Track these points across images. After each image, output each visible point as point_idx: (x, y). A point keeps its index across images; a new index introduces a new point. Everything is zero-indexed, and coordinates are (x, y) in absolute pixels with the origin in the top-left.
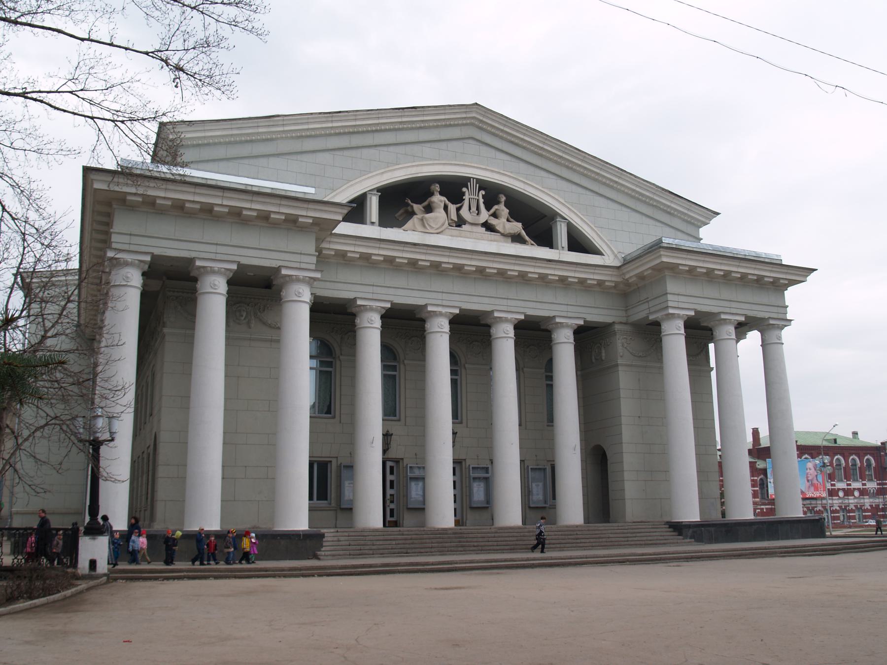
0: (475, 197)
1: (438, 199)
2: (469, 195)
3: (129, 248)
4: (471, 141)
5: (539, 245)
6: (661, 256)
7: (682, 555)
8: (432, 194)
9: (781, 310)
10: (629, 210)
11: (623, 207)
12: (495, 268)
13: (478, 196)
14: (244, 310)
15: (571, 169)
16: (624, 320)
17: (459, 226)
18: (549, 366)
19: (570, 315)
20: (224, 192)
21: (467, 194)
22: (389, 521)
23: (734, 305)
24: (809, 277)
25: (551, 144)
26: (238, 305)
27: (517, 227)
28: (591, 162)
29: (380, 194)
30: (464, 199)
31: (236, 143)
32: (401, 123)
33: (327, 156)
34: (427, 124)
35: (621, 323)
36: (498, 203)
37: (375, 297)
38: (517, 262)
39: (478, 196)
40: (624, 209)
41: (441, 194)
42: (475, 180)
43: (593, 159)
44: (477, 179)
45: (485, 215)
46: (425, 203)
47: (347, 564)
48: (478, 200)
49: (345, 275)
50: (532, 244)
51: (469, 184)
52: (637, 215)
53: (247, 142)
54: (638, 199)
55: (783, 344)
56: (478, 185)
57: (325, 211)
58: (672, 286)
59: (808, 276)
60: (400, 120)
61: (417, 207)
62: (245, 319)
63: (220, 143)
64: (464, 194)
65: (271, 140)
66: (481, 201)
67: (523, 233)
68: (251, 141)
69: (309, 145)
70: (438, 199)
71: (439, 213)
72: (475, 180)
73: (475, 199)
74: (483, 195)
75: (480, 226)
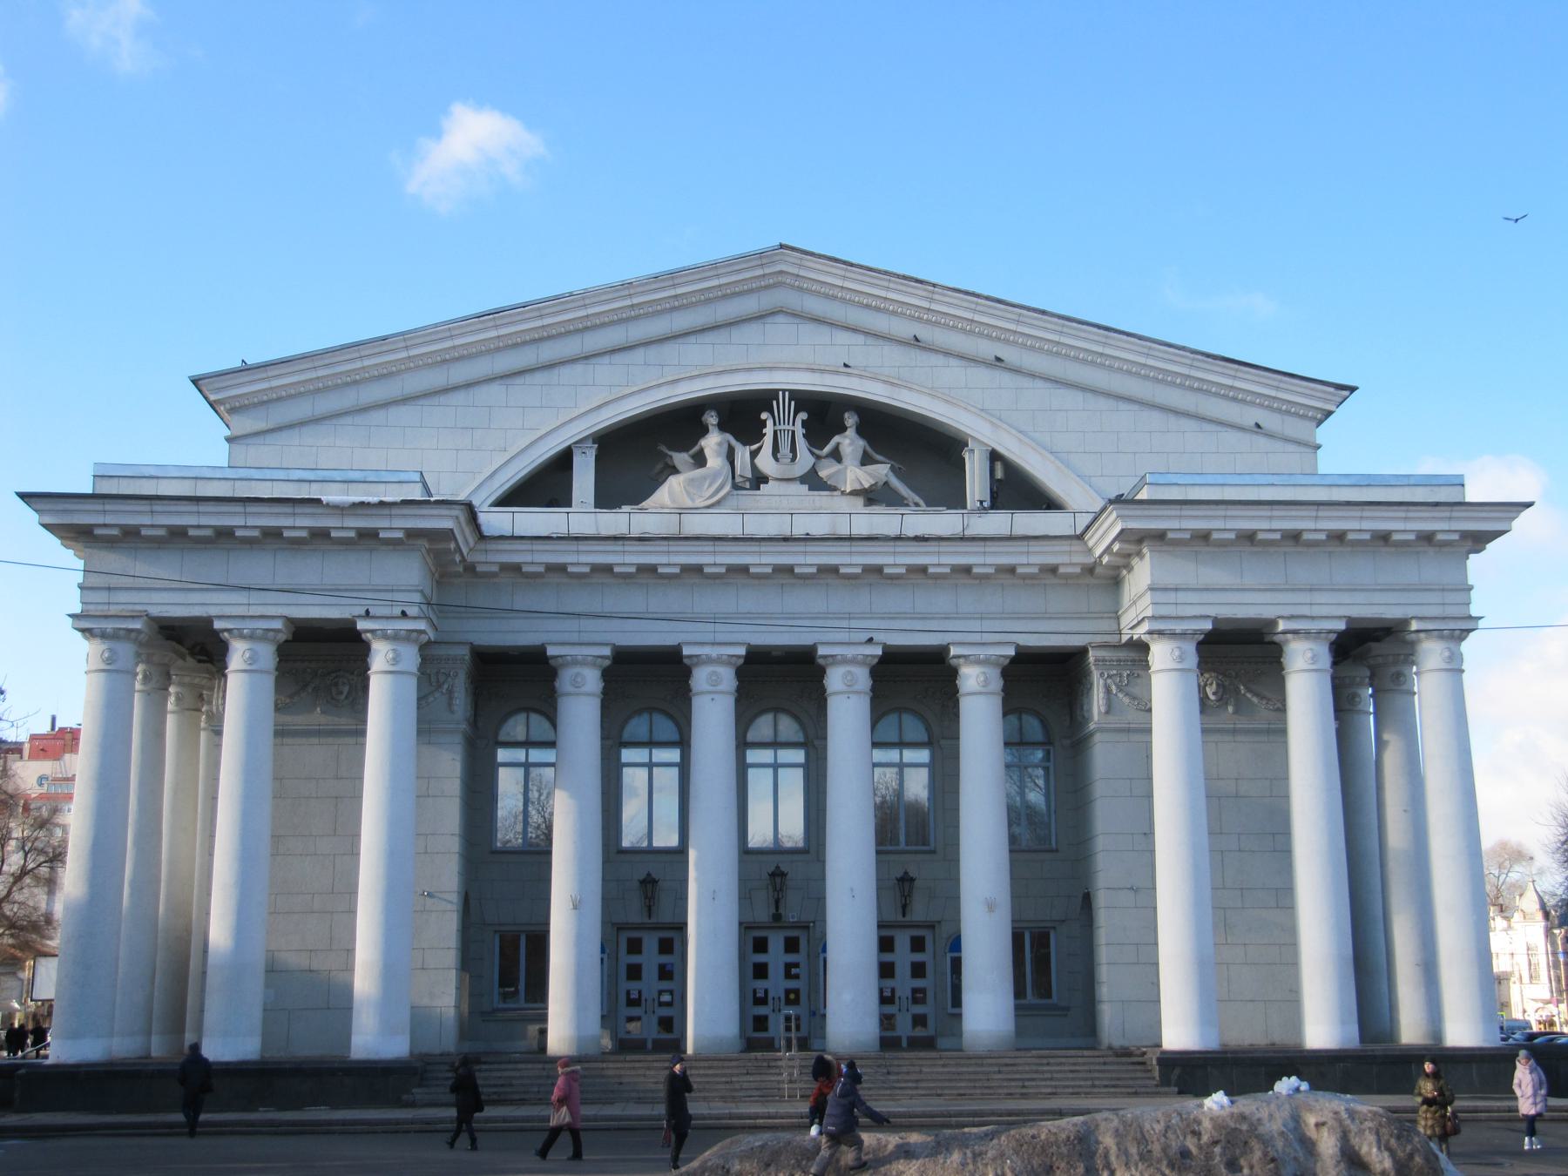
0: (786, 427)
2: (775, 424)
4: (780, 319)
5: (928, 505)
7: (1496, 1114)
8: (704, 431)
9: (1458, 597)
10: (1136, 407)
11: (1120, 403)
12: (811, 565)
13: (794, 424)
14: (344, 683)
20: (245, 506)
21: (770, 423)
26: (334, 675)
27: (882, 471)
28: (1035, 322)
29: (596, 446)
30: (765, 434)
31: (327, 389)
33: (495, 390)
34: (685, 301)
36: (842, 429)
39: (794, 424)
40: (1123, 406)
41: (722, 427)
42: (787, 393)
43: (1040, 316)
44: (790, 391)
45: (805, 459)
47: (1047, 1107)
48: (793, 432)
50: (917, 505)
51: (775, 403)
52: (1156, 416)
53: (347, 384)
55: (1463, 671)
56: (793, 403)
57: (423, 516)
59: (1514, 519)
60: (628, 302)
61: (680, 458)
62: (346, 698)
63: (301, 394)
65: (391, 374)
66: (800, 431)
67: (896, 483)
68: (355, 382)
69: (461, 373)
70: (713, 443)
71: (715, 461)
72: (787, 393)
73: (788, 430)
74: (803, 421)
75: (798, 482)
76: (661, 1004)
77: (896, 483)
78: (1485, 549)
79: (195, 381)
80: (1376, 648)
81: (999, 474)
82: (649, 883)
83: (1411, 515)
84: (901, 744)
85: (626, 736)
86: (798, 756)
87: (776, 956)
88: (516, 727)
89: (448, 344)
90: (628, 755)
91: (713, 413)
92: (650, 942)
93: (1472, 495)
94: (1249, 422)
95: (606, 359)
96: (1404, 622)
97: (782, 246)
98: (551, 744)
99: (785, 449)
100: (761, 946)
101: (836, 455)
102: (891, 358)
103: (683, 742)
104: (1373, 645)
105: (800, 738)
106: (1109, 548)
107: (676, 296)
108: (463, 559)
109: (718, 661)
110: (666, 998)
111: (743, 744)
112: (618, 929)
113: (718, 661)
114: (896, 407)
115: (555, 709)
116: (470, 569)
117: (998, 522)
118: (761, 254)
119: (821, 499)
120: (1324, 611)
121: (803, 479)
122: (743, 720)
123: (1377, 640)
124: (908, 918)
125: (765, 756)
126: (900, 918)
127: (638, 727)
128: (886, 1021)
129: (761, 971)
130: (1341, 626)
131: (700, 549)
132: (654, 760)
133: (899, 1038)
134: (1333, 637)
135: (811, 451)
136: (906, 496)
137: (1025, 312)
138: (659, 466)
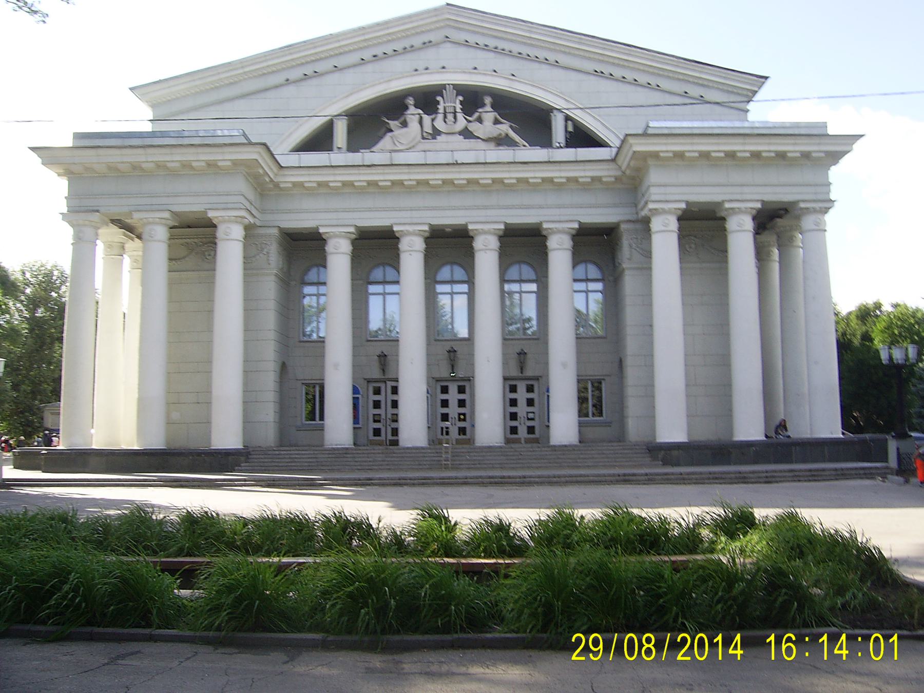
1: (413, 113)
3: (300, 162)
6: (631, 146)
15: (569, 54)
16: (633, 217)
17: (434, 138)
18: (209, 313)
19: (563, 218)
22: (390, 440)
23: (746, 189)
24: (856, 144)
25: (539, 31)
27: (505, 128)
31: (321, 59)
32: (365, 40)
35: (629, 221)
37: (340, 222)
38: (487, 169)
41: (416, 106)
45: (462, 122)
46: (402, 119)
49: (308, 203)
50: (524, 146)
54: (659, 75)
55: (825, 231)
58: (655, 176)
59: (853, 144)
60: (363, 38)
61: (393, 124)
64: (438, 103)
66: (459, 107)
67: (512, 134)
70: (413, 113)
74: (461, 101)
76: (529, 419)
77: (512, 134)
78: (838, 162)
79: (131, 89)
80: (779, 221)
81: (570, 129)
82: (383, 357)
83: (797, 141)
84: (587, 280)
85: (439, 278)
86: (533, 287)
87: (522, 395)
88: (378, 274)
89: (265, 64)
90: (440, 288)
91: (411, 98)
92: (453, 388)
93: (831, 131)
94: (681, 91)
95: (351, 70)
96: (794, 204)
97: (448, 4)
98: (397, 282)
99: (450, 117)
100: (513, 389)
101: (480, 120)
102: (507, 65)
103: (470, 281)
104: (778, 220)
105: (534, 278)
106: (629, 164)
107: (388, 34)
108: (272, 181)
109: (413, 234)
110: (531, 416)
111: (503, 280)
112: (368, 382)
113: (413, 234)
114: (422, 86)
115: (399, 263)
116: (277, 185)
117: (570, 154)
118: (436, 10)
119: (472, 143)
120: (749, 197)
121: (460, 133)
122: (504, 267)
123: (780, 217)
124: (524, 375)
125: (446, 288)
126: (520, 375)
127: (445, 273)
128: (356, 436)
129: (513, 402)
130: (759, 205)
131: (401, 171)
132: (386, 291)
133: (520, 439)
134: (754, 212)
135: (465, 118)
136: (518, 141)
137: (583, 37)
138: (384, 130)
